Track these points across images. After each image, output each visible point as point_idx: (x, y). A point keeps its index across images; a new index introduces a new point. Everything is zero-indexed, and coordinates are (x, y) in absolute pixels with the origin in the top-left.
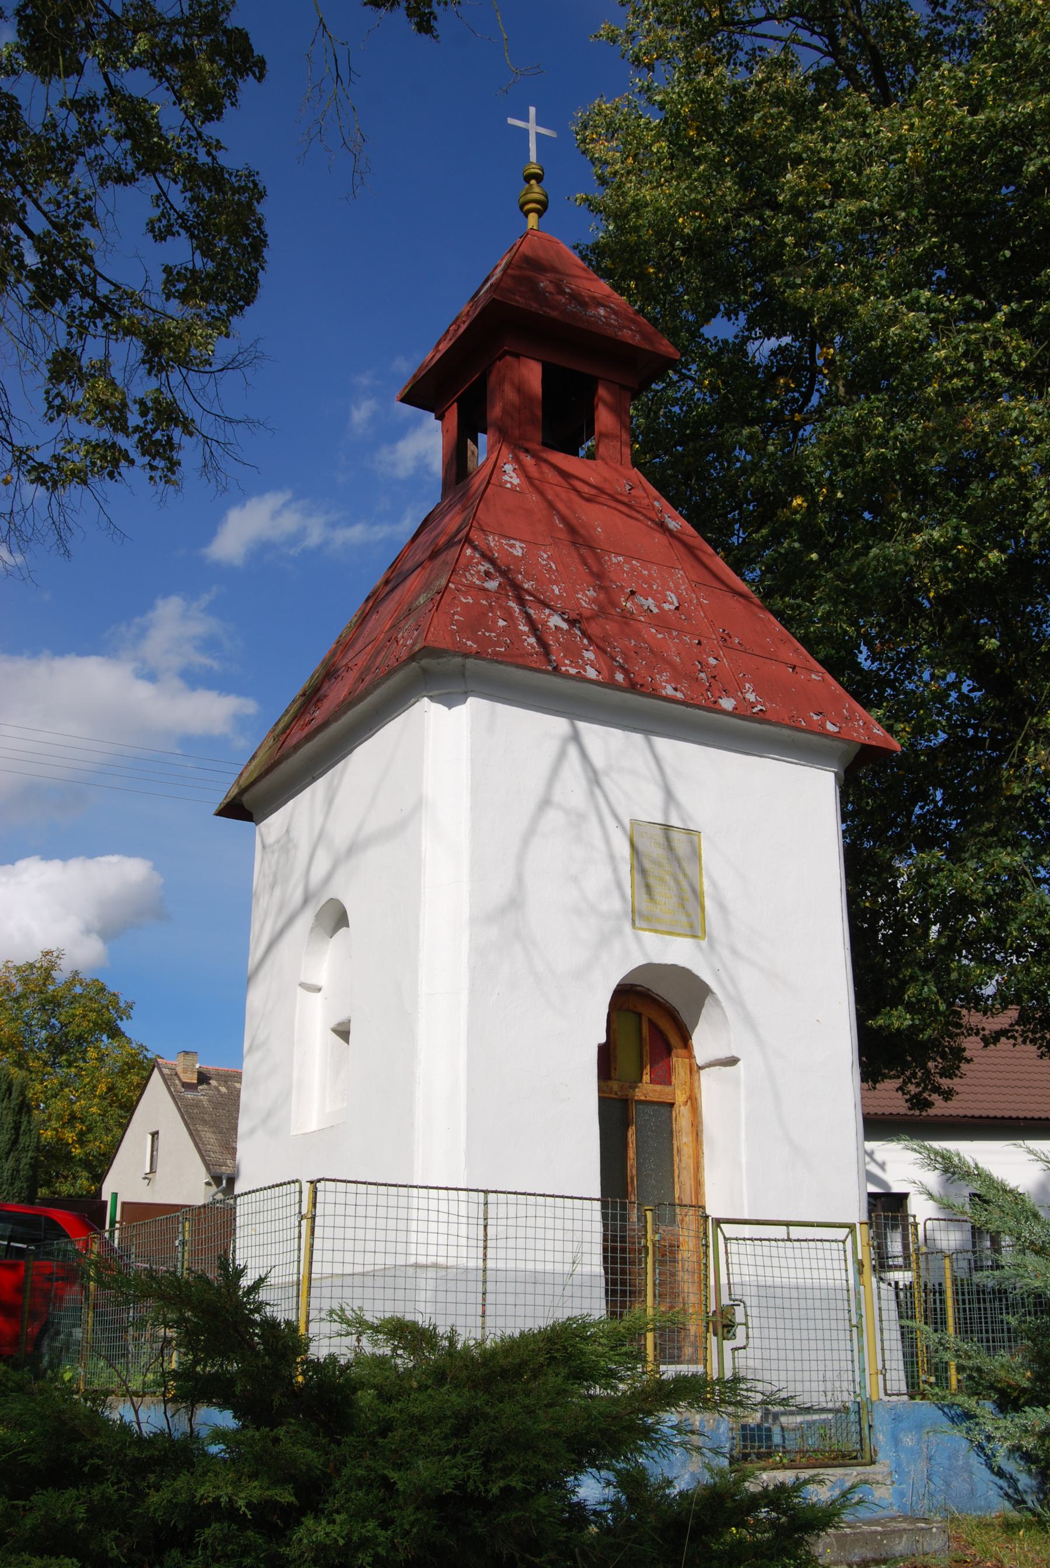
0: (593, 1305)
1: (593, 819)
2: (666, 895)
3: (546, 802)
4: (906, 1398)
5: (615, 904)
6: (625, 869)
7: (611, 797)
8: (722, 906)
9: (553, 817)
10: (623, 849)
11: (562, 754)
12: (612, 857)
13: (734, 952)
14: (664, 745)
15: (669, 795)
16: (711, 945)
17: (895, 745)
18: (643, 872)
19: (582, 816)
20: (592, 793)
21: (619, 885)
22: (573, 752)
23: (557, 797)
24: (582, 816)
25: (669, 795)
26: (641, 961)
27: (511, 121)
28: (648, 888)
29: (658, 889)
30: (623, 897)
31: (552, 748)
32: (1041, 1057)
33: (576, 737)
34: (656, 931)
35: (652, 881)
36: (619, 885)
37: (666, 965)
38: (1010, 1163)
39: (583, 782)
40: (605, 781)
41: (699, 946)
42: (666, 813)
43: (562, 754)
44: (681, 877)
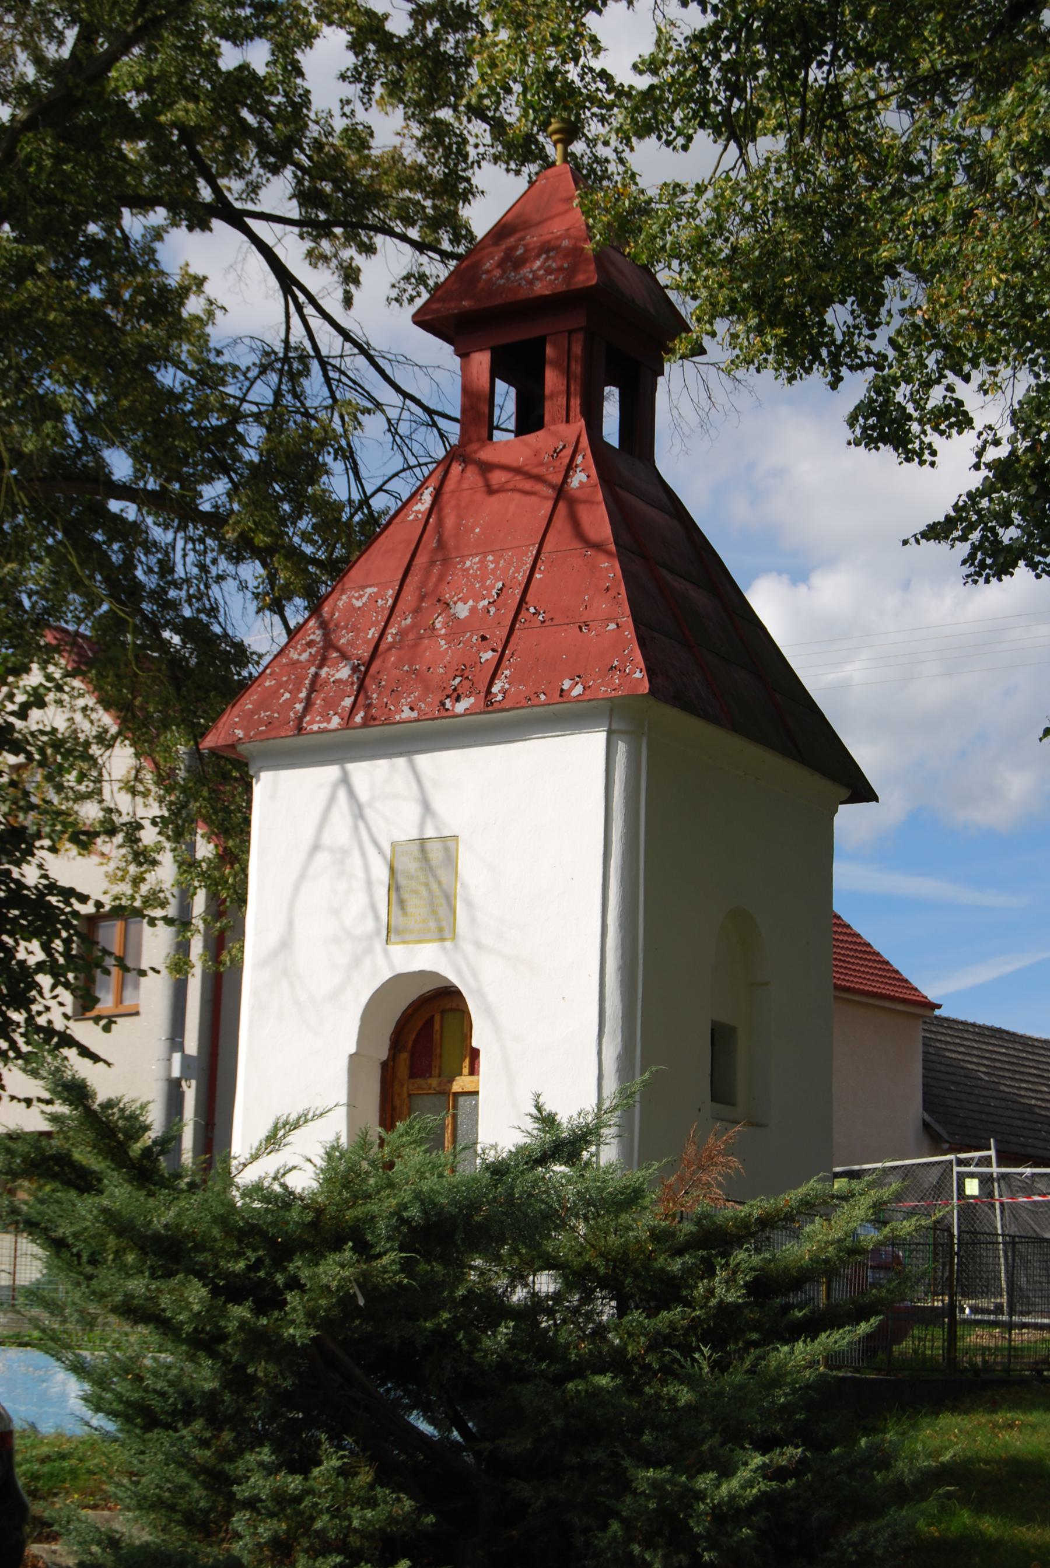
0: (299, 56)
1: (356, 853)
2: (417, 906)
3: (316, 848)
4: (512, 436)
5: (370, 925)
6: (381, 893)
7: (374, 829)
8: (469, 904)
9: (323, 858)
10: (381, 873)
11: (332, 799)
12: (369, 883)
13: (478, 945)
14: (425, 761)
15: (427, 808)
16: (456, 946)
17: (895, 1348)
18: (398, 889)
19: (345, 852)
20: (356, 828)
21: (374, 907)
22: (342, 794)
23: (326, 839)
24: (345, 852)
25: (427, 808)
26: (387, 975)
27: (361, 1302)
28: (401, 903)
29: (410, 909)
30: (377, 918)
31: (324, 794)
32: (791, 379)
33: (345, 780)
34: (404, 942)
35: (406, 896)
36: (374, 907)
37: (409, 973)
38: (622, 44)
39: (349, 819)
40: (368, 812)
41: (444, 948)
42: (422, 826)
43: (332, 799)
44: (434, 886)
